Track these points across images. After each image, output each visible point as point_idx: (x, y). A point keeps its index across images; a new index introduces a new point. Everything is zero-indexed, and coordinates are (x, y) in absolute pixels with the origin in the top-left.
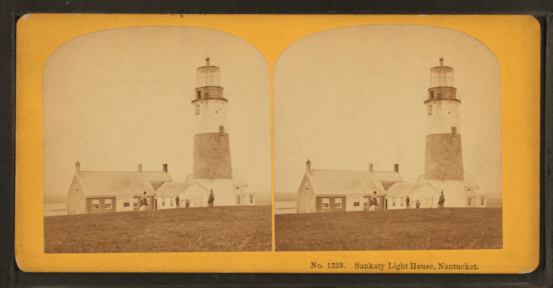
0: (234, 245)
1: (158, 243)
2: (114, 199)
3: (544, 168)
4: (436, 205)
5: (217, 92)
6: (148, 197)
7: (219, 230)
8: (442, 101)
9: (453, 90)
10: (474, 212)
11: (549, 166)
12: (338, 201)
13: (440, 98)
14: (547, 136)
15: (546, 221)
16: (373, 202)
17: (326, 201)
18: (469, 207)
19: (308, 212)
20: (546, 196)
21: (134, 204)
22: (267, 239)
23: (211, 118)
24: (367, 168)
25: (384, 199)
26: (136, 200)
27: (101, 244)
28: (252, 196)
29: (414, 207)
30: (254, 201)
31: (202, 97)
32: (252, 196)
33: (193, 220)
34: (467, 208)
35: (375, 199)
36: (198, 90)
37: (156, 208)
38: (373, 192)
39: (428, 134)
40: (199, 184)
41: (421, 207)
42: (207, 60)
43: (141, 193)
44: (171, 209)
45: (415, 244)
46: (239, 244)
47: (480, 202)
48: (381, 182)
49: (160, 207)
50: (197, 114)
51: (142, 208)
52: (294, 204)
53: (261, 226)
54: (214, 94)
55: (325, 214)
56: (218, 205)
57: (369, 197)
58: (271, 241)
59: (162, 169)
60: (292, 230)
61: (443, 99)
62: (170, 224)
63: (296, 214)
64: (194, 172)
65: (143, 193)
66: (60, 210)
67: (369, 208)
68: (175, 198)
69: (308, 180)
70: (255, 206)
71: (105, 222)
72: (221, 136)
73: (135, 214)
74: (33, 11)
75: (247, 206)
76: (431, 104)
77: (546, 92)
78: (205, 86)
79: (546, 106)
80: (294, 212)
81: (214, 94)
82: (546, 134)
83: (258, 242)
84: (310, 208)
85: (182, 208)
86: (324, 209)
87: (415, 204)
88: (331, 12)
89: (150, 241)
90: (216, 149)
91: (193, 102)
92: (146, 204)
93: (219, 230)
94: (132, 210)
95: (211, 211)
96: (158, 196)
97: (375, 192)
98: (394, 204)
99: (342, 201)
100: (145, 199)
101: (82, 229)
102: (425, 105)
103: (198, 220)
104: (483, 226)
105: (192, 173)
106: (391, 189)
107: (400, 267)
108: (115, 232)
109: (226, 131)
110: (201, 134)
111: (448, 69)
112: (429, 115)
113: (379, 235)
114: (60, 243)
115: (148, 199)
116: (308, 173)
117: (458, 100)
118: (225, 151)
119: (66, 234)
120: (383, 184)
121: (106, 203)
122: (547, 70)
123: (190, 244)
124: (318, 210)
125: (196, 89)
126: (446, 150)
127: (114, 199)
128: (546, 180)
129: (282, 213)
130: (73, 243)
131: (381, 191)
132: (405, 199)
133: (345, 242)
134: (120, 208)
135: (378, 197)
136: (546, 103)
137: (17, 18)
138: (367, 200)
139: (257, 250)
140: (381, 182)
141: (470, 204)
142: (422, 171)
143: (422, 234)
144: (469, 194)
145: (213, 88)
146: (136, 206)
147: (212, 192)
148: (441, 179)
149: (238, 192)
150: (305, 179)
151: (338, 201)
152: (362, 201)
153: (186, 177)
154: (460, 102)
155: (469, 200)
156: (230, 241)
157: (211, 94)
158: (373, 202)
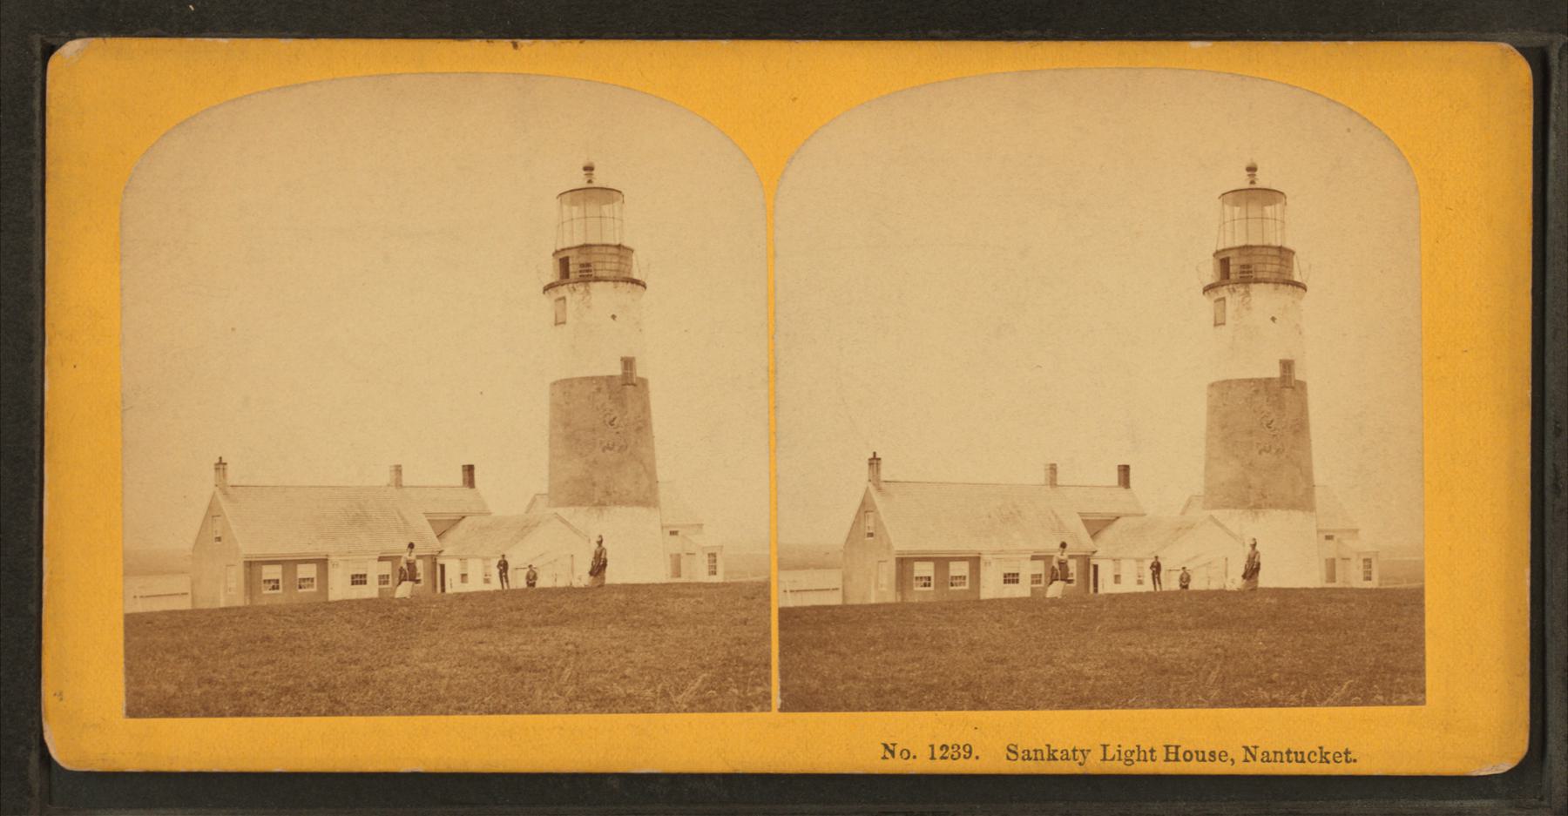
0: (665, 693)
1: (448, 688)
2: (322, 563)
4: (1235, 582)
5: (616, 259)
6: (419, 557)
7: (620, 651)
8: (1255, 288)
9: (1284, 254)
10: (1345, 602)
11: (1556, 471)
12: (959, 569)
13: (1248, 278)
16: (1059, 573)
17: (924, 569)
20: (1548, 556)
21: (381, 577)
22: (758, 676)
23: (599, 333)
24: (1041, 477)
25: (1087, 563)
26: (386, 568)
27: (287, 690)
28: (714, 555)
29: (1174, 585)
30: (720, 569)
31: (572, 276)
32: (714, 555)
33: (546, 623)
34: (1323, 589)
35: (1062, 564)
36: (562, 255)
37: (443, 590)
38: (1057, 545)
40: (563, 521)
42: (586, 169)
43: (399, 546)
44: (484, 593)
45: (1177, 692)
46: (678, 693)
47: (1360, 573)
49: (454, 586)
50: (559, 322)
51: (404, 590)
52: (833, 578)
53: (739, 641)
54: (608, 266)
55: (921, 607)
56: (619, 581)
58: (770, 684)
59: (458, 478)
61: (1257, 281)
62: (482, 635)
63: (840, 607)
64: (550, 487)
65: (405, 546)
66: (169, 595)
67: (1045, 590)
68: (495, 562)
69: (874, 509)
70: (724, 585)
72: (626, 384)
73: (382, 607)
74: (93, 31)
75: (699, 585)
76: (1221, 295)
77: (1550, 262)
78: (581, 243)
79: (1548, 300)
81: (606, 266)
82: (1548, 380)
83: (731, 686)
84: (878, 588)
85: (515, 591)
86: (918, 593)
87: (1176, 577)
88: (939, 33)
89: (424, 683)
90: (611, 423)
91: (547, 289)
92: (413, 578)
93: (620, 651)
94: (375, 594)
95: (598, 598)
97: (1063, 545)
98: (1117, 578)
99: (971, 569)
100: (411, 565)
101: (233, 650)
102: (1204, 298)
103: (561, 623)
105: (545, 490)
106: (1108, 534)
108: (325, 658)
109: (640, 372)
111: (1271, 195)
112: (1216, 325)
114: (171, 689)
115: (420, 564)
116: (872, 489)
117: (1298, 285)
118: (639, 429)
119: (187, 663)
120: (1086, 522)
121: (300, 576)
122: (1550, 197)
124: (903, 594)
125: (557, 252)
126: (1265, 424)
127: (322, 563)
129: (799, 604)
130: (206, 687)
131: (1081, 541)
132: (1149, 563)
133: (980, 687)
134: (340, 588)
135: (1071, 557)
136: (1549, 290)
137: (49, 51)
138: (1040, 568)
139: (730, 709)
142: (1197, 485)
143: (1197, 662)
144: (1330, 549)
146: (386, 582)
147: (600, 543)
148: (1251, 508)
149: (675, 545)
150: (866, 508)
151: (959, 569)
152: (1027, 569)
153: (528, 501)
155: (1331, 565)
156: (651, 684)
157: (599, 266)
158: (1059, 573)
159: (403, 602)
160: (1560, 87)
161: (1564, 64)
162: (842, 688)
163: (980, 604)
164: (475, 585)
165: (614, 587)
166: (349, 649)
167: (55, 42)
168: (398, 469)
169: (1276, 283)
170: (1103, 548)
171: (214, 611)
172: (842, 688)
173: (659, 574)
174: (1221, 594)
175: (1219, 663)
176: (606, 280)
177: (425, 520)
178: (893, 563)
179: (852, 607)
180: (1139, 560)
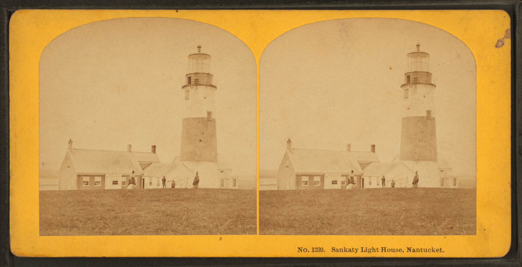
0: (217, 226)
1: (144, 220)
2: (103, 177)
3: (515, 149)
9: (428, 74)
11: (520, 148)
12: (317, 179)
13: (416, 82)
14: (518, 119)
15: (518, 200)
18: (442, 187)
19: (288, 189)
21: (123, 182)
22: (249, 221)
23: (201, 102)
25: (360, 178)
26: (125, 179)
28: (235, 180)
31: (192, 83)
32: (235, 180)
36: (189, 76)
37: (143, 188)
38: (131, 172)
39: (404, 117)
40: (185, 166)
41: (396, 186)
42: (198, 47)
43: (129, 172)
44: (232, 190)
46: (221, 226)
48: (358, 161)
49: (147, 186)
51: (131, 187)
52: (274, 181)
54: (204, 80)
55: (304, 192)
57: (346, 176)
59: (150, 149)
60: (270, 209)
61: (419, 83)
62: (156, 203)
68: (161, 179)
71: (94, 199)
72: (208, 120)
73: (122, 193)
76: (407, 88)
77: (517, 76)
79: (517, 90)
80: (275, 188)
81: (203, 80)
82: (517, 117)
83: (240, 224)
84: (290, 185)
85: (167, 189)
86: (303, 187)
90: (203, 133)
91: (402, 86)
92: (134, 183)
95: (195, 193)
96: (365, 176)
98: (370, 183)
100: (133, 178)
101: (72, 205)
102: (401, 89)
104: (452, 208)
105: (179, 155)
106: (368, 168)
107: (372, 251)
108: (103, 208)
109: (213, 117)
110: (409, 117)
113: (137, 213)
114: (50, 217)
115: (136, 178)
117: (213, 86)
118: (212, 136)
120: (360, 164)
121: (96, 180)
122: (517, 56)
123: (174, 223)
125: (187, 75)
126: (421, 131)
127: (103, 177)
128: (518, 161)
131: (358, 170)
132: (381, 178)
133: (323, 219)
134: (109, 185)
135: (355, 176)
136: (517, 87)
137: (10, 15)
138: (344, 179)
140: (358, 161)
141: (443, 185)
143: (397, 212)
145: (203, 75)
146: (124, 184)
147: (197, 174)
150: (286, 157)
151: (317, 179)
152: (340, 179)
154: (435, 86)
156: (212, 222)
157: (201, 80)
158: (351, 181)
159: (130, 191)
160: (519, 18)
161: (521, 10)
162: (277, 218)
163: (324, 191)
164: (154, 186)
165: (200, 189)
166: (110, 206)
167: (11, 10)
168: (130, 146)
169: (426, 84)
170: (366, 174)
171: (66, 191)
172: (277, 218)
173: (217, 185)
174: (405, 189)
175: (404, 212)
176: (203, 85)
177: (138, 163)
178: (295, 177)
179: (281, 191)
180: (377, 177)
